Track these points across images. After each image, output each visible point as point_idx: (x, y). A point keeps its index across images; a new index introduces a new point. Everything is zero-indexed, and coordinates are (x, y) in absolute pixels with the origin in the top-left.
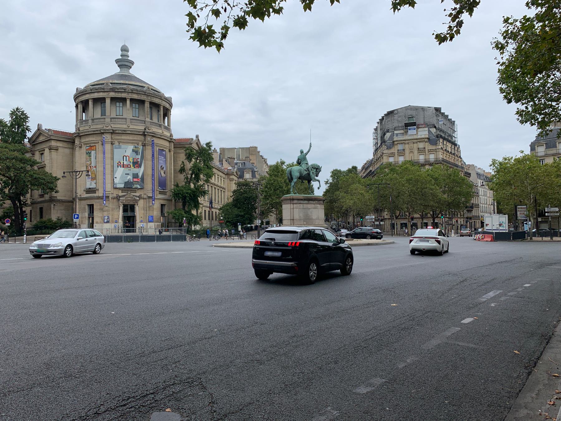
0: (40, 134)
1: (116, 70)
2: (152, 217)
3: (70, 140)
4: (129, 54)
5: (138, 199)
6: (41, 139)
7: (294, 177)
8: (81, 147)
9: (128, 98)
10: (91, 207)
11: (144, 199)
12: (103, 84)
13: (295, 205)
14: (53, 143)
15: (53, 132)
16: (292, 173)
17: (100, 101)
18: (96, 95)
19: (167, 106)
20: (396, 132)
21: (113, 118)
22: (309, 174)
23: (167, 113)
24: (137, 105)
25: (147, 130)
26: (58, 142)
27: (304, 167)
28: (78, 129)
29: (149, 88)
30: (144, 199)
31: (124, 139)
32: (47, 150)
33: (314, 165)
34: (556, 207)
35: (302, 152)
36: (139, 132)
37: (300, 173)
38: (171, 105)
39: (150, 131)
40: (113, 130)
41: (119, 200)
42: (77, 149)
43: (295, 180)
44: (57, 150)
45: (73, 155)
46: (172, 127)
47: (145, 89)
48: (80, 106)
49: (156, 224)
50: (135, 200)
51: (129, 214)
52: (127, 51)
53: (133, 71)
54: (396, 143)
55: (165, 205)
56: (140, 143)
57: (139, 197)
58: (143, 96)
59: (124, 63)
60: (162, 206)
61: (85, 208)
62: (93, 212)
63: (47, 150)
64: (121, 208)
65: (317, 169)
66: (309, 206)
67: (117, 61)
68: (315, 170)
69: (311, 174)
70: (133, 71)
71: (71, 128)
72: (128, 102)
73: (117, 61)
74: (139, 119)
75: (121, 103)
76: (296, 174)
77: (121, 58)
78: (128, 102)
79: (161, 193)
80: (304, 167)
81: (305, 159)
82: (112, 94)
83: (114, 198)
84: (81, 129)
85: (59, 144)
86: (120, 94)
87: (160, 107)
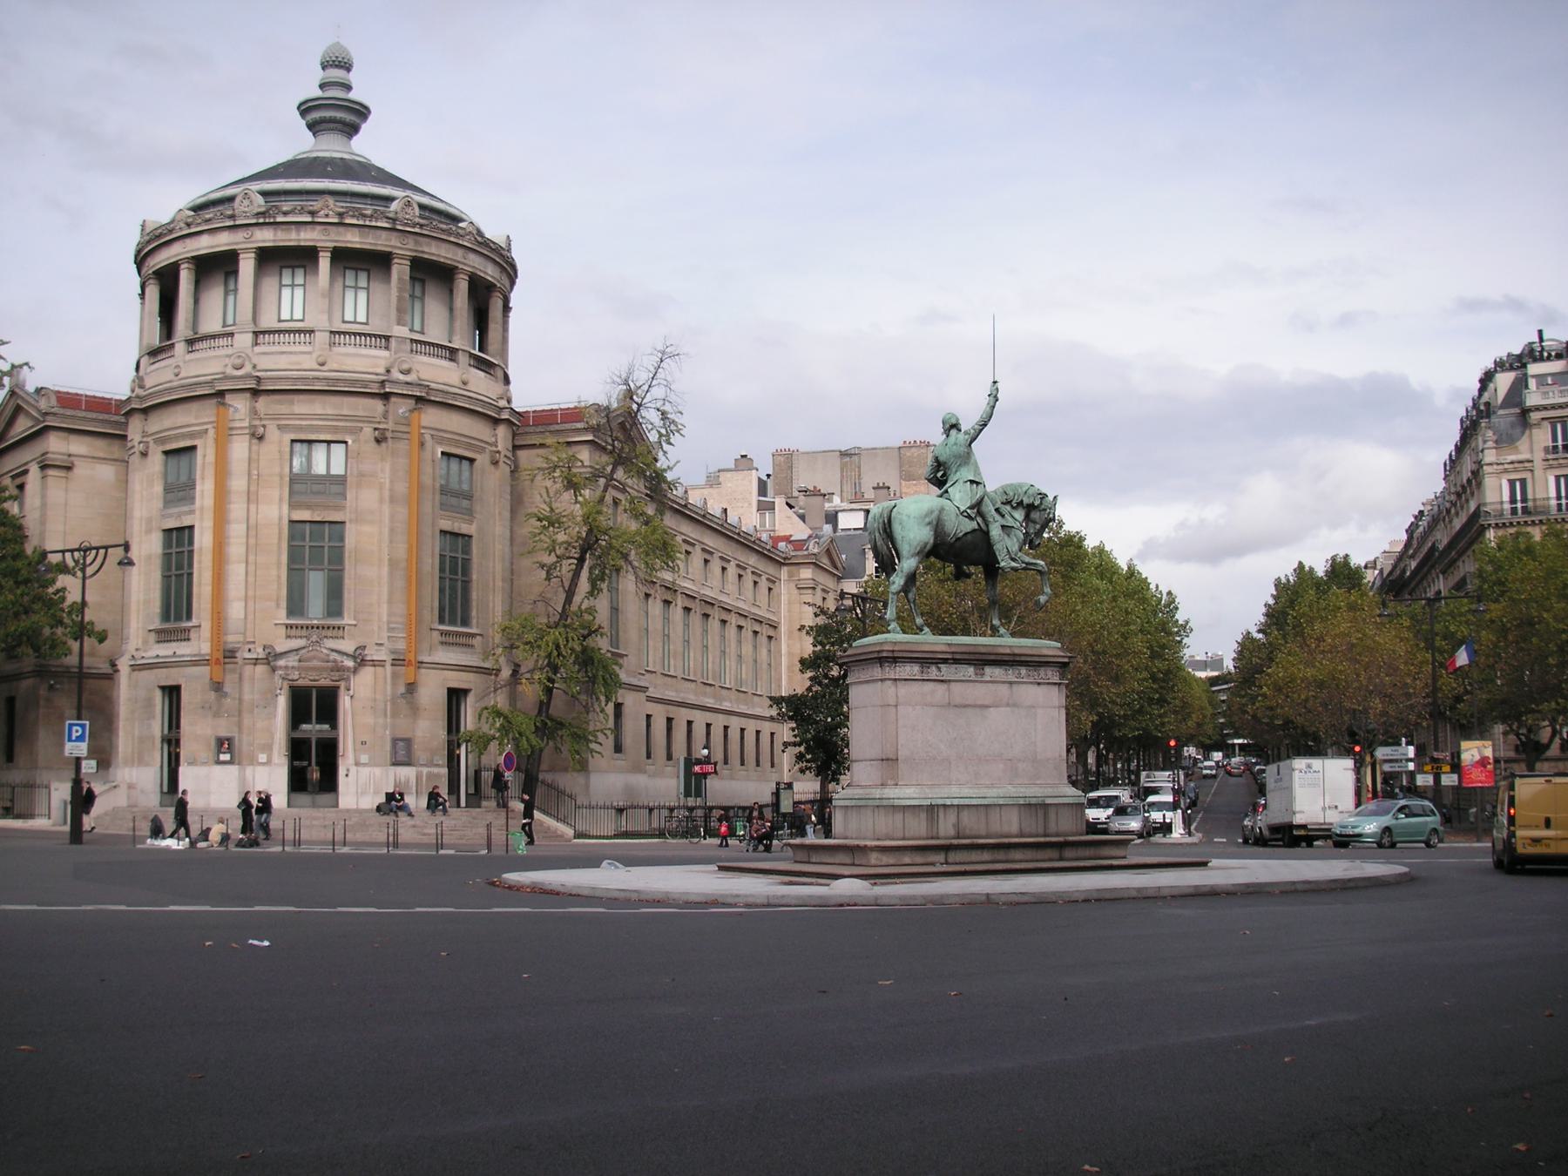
0: (18, 410)
1: (300, 142)
2: (408, 742)
3: (106, 421)
4: (353, 77)
5: (350, 663)
6: (22, 426)
7: (905, 549)
8: (144, 454)
9: (325, 249)
10: (173, 693)
11: (374, 663)
12: (231, 199)
13: (904, 690)
14: (55, 445)
15: (54, 402)
16: (897, 528)
17: (217, 267)
18: (205, 245)
19: (490, 272)
20: (1534, 369)
21: (264, 333)
22: (984, 534)
23: (486, 301)
24: (363, 277)
25: (396, 375)
26: (73, 437)
27: (960, 496)
28: (139, 381)
29: (409, 204)
30: (374, 663)
31: (302, 417)
32: (34, 470)
33: (1015, 487)
34: (1049, 636)
35: (952, 426)
36: (365, 383)
37: (938, 527)
38: (509, 270)
39: (408, 378)
40: (259, 379)
41: (274, 670)
42: (135, 460)
43: (908, 564)
44: (69, 468)
45: (124, 482)
46: (515, 367)
47: (394, 206)
48: (153, 292)
49: (425, 770)
50: (338, 668)
51: (313, 729)
52: (347, 66)
53: (367, 145)
54: (1535, 416)
55: (465, 692)
56: (368, 431)
57: (354, 657)
58: (384, 234)
59: (336, 113)
60: (455, 697)
61: (149, 703)
62: (178, 727)
63: (34, 470)
64: (282, 703)
65: (1030, 508)
66: (978, 693)
67: (305, 109)
68: (1019, 515)
69: (995, 532)
70: (367, 145)
71: (114, 381)
72: (324, 263)
73: (305, 109)
74: (366, 329)
75: (300, 273)
76: (913, 534)
77: (319, 93)
78: (324, 263)
79: (449, 641)
80: (960, 496)
81: (966, 457)
82: (266, 237)
83: (256, 661)
84: (149, 382)
85: (78, 446)
86: (293, 235)
87: (469, 282)
